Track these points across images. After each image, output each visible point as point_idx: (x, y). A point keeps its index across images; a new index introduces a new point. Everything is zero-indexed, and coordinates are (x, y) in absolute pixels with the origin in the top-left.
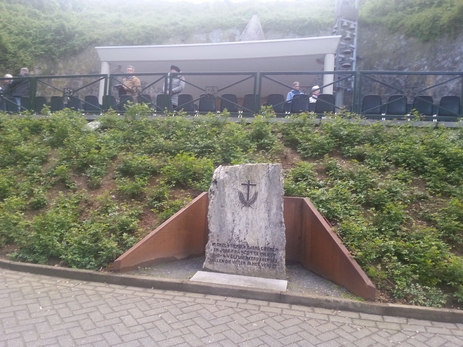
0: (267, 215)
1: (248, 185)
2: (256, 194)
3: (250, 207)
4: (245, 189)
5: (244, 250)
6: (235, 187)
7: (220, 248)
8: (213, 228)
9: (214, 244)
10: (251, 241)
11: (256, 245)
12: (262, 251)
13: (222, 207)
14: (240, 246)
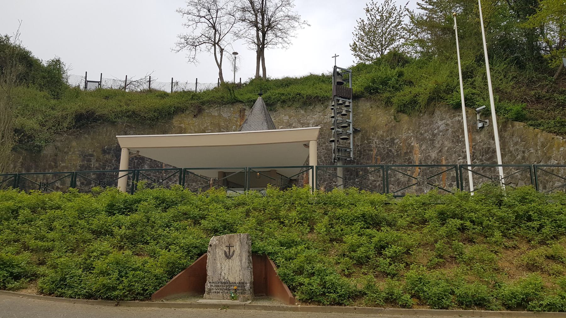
1: (229, 247)
2: (234, 251)
8: (209, 273)
9: (210, 283)
10: (231, 280)
14: (225, 283)
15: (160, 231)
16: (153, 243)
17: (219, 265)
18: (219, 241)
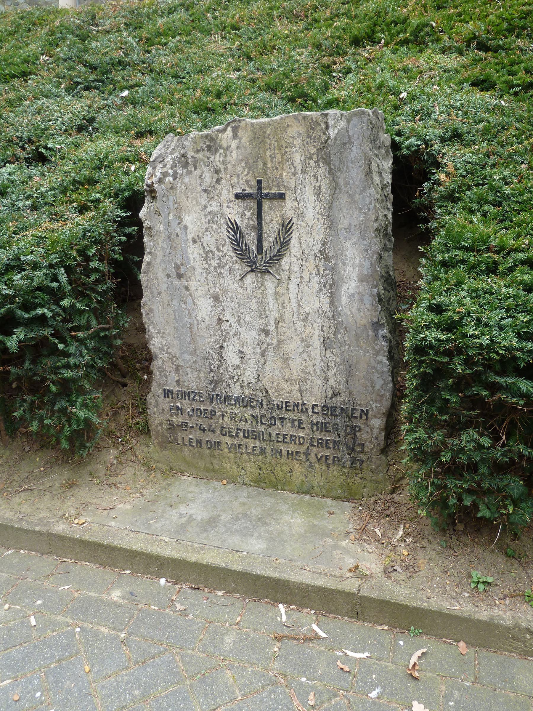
0: (325, 300)
2: (286, 228)
3: (267, 277)
4: (248, 214)
5: (257, 412)
6: (214, 207)
7: (186, 404)
9: (167, 393)
11: (296, 397)
12: (315, 419)
13: (180, 276)
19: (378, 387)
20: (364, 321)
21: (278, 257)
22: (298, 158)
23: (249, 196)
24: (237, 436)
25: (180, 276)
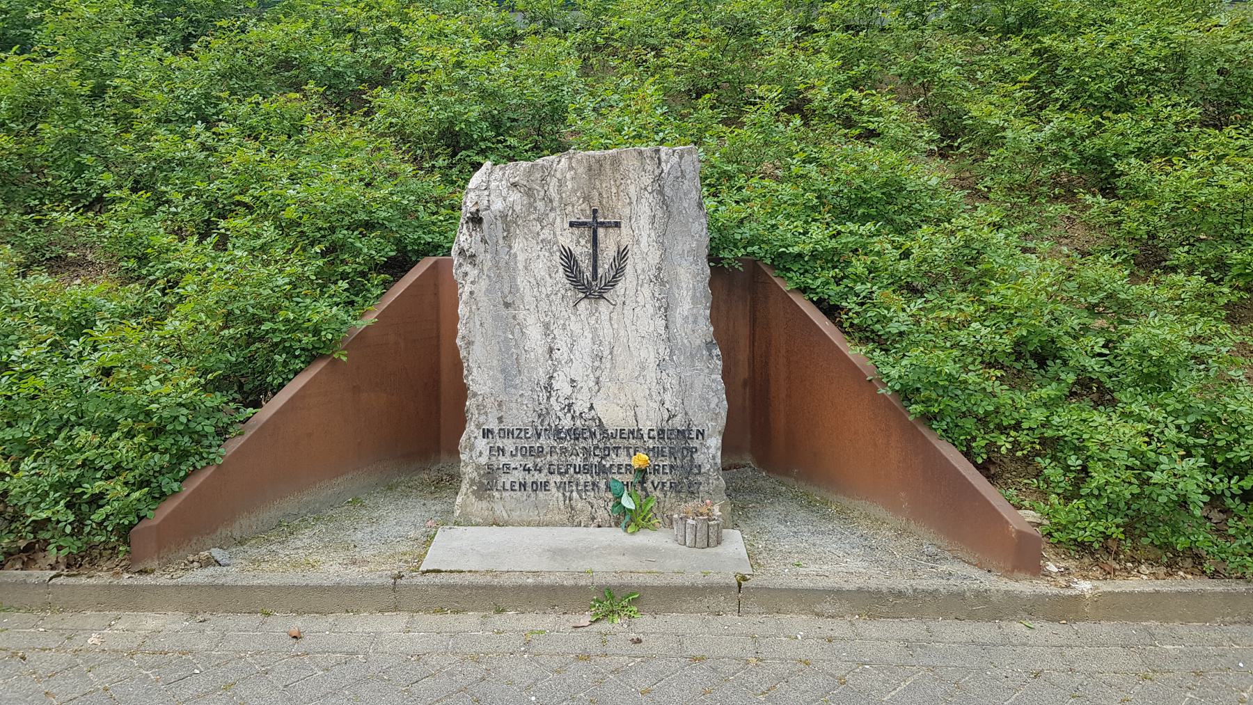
1: (593, 226)
2: (622, 255)
3: (602, 302)
5: (590, 443)
7: (509, 445)
8: (480, 379)
9: (487, 433)
10: (613, 415)
12: (651, 444)
14: (575, 434)
15: (163, 142)
16: (129, 204)
17: (534, 332)
18: (529, 193)
19: (713, 406)
20: (698, 342)
21: (613, 283)
22: (632, 190)
23: (584, 224)
24: (566, 472)
25: (507, 305)
